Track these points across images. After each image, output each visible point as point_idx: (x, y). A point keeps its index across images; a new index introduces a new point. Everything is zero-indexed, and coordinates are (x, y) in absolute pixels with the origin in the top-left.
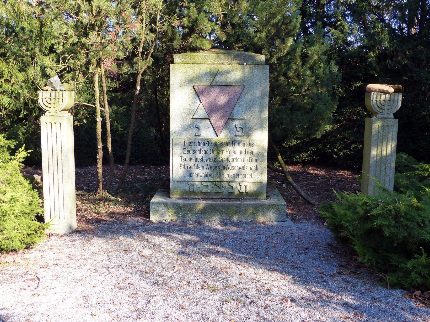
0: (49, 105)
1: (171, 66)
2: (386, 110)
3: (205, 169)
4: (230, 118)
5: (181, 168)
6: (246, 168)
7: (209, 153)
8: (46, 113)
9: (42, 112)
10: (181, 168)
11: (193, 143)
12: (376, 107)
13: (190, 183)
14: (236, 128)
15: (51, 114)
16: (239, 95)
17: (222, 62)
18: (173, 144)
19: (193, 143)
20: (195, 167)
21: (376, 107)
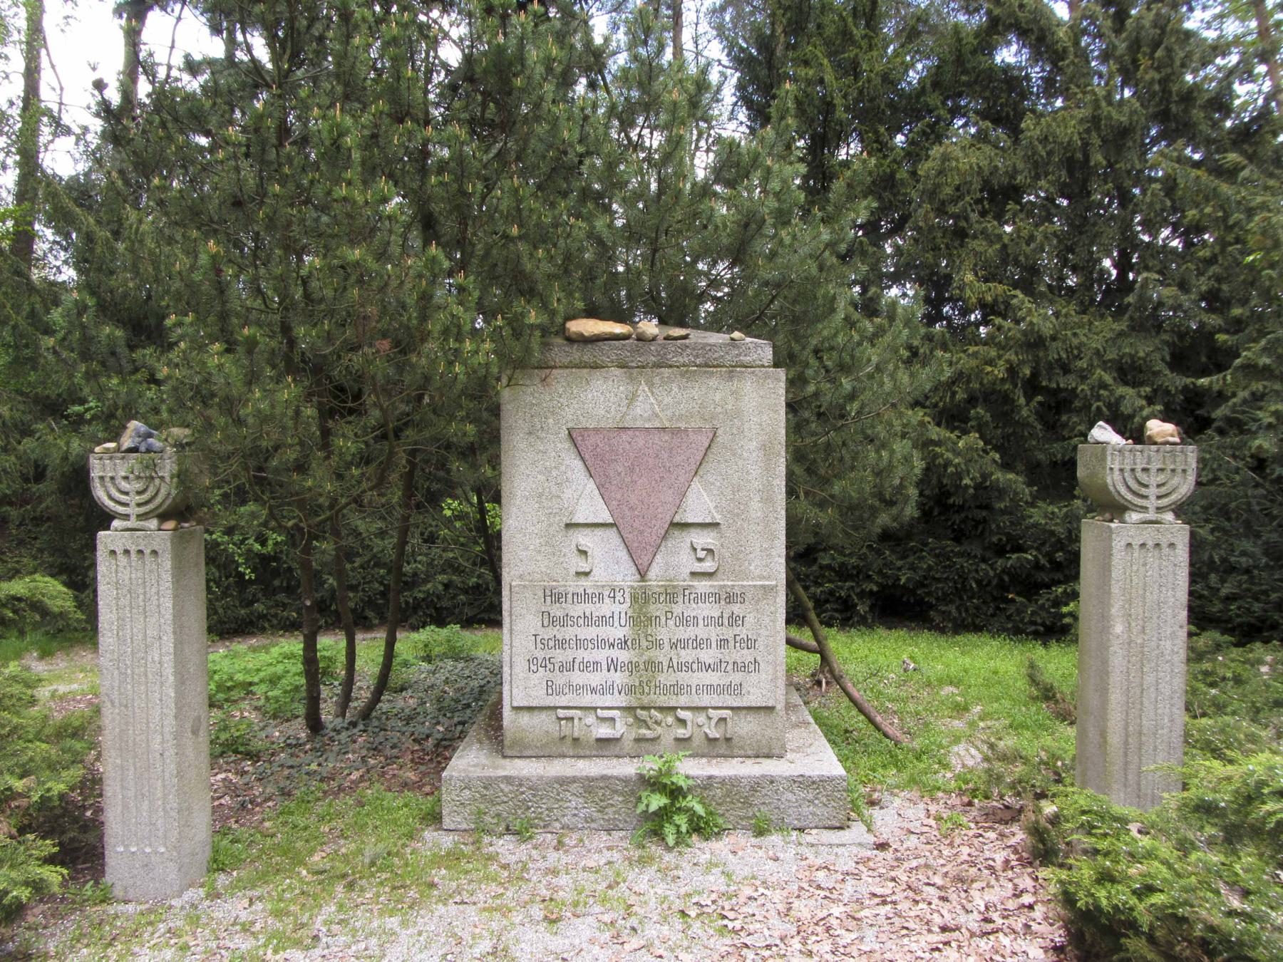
0: (123, 498)
1: (157, 9)
2: (1153, 498)
3: (605, 671)
4: (675, 521)
5: (534, 668)
6: (724, 665)
7: (616, 624)
8: (116, 523)
9: (104, 519)
10: (534, 668)
11: (570, 596)
12: (1123, 490)
13: (561, 713)
14: (695, 550)
15: (128, 524)
16: (702, 454)
17: (168, 502)
18: (511, 615)
19: (570, 596)
20: (576, 667)
21: (1123, 490)
